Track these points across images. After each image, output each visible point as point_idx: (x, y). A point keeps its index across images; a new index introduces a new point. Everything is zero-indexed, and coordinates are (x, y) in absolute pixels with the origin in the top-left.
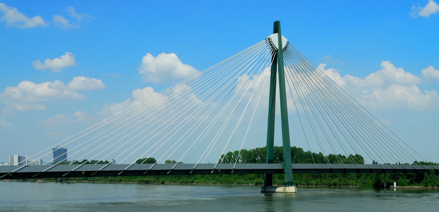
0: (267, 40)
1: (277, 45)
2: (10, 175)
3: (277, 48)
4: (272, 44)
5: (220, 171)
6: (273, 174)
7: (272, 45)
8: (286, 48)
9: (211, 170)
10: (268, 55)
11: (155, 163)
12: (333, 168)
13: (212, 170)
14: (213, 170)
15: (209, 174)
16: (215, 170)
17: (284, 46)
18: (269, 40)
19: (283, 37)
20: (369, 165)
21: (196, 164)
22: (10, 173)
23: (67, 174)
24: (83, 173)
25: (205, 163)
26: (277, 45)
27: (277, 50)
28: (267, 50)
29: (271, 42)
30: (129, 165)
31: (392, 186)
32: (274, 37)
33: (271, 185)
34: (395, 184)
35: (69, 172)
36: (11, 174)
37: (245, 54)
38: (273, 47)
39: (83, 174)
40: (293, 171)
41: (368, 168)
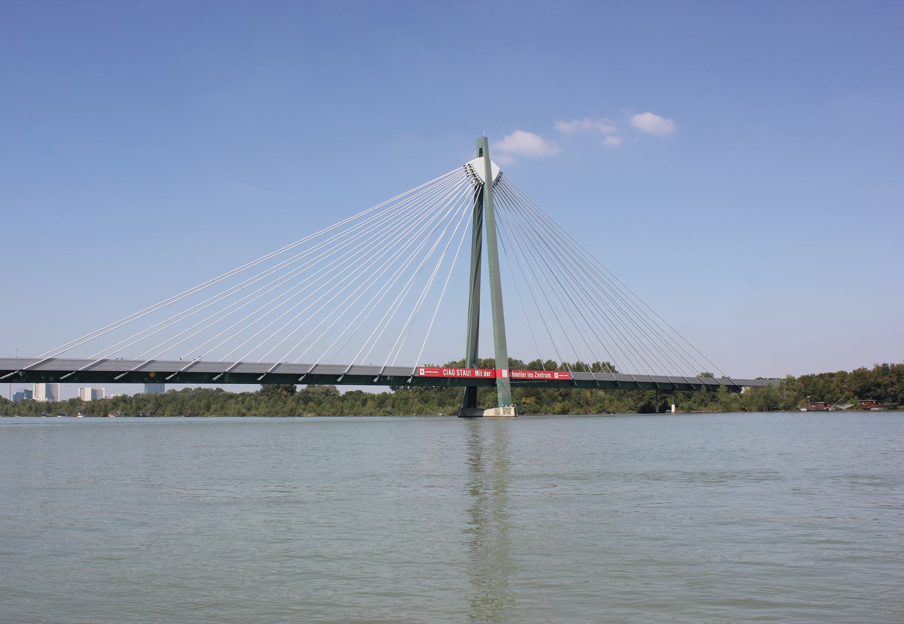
0: (468, 173)
1: (483, 177)
2: (21, 374)
3: (482, 181)
4: (477, 178)
5: (389, 378)
6: (744, 386)
7: (477, 179)
8: (498, 180)
9: (375, 377)
10: (470, 191)
11: (523, 383)
12: (598, 380)
13: (376, 376)
14: (341, 376)
15: (406, 384)
16: (381, 376)
17: (494, 177)
18: (472, 171)
19: (492, 164)
20: (652, 376)
21: (312, 365)
22: (20, 371)
23: (173, 375)
24: (152, 375)
25: (365, 365)
26: (483, 177)
27: (482, 183)
28: (468, 188)
29: (479, 179)
30: (233, 364)
31: (669, 411)
32: (478, 164)
33: (475, 406)
34: (673, 407)
35: (74, 371)
36: (21, 372)
37: (434, 198)
38: (481, 183)
39: (152, 377)
40: (512, 385)
41: (668, 382)
